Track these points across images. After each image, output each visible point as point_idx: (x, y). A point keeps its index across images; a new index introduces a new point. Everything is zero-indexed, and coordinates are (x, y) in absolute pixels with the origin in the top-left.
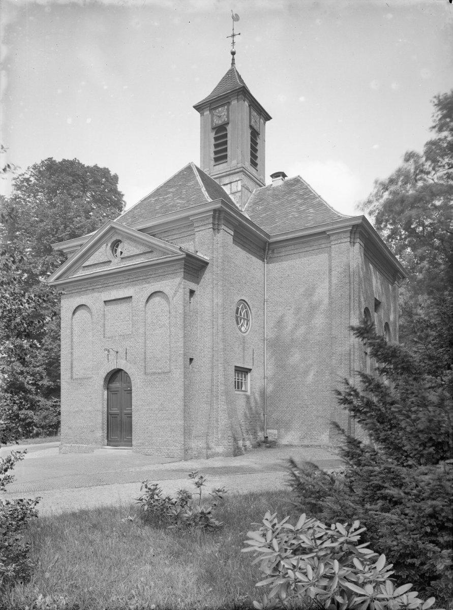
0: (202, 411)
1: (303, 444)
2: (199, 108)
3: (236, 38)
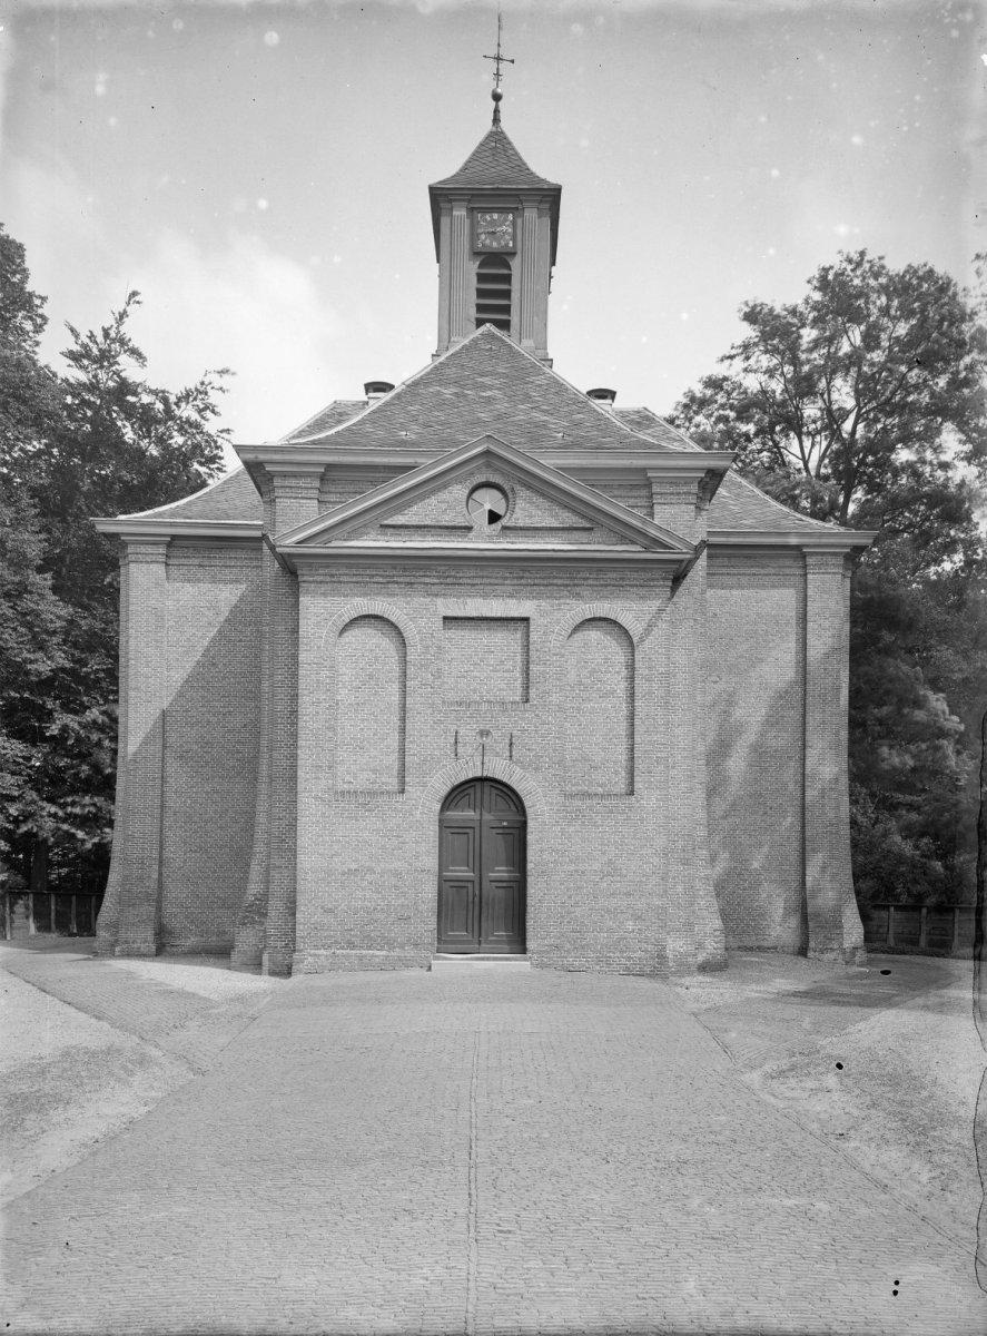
0: (674, 878)
1: (741, 944)
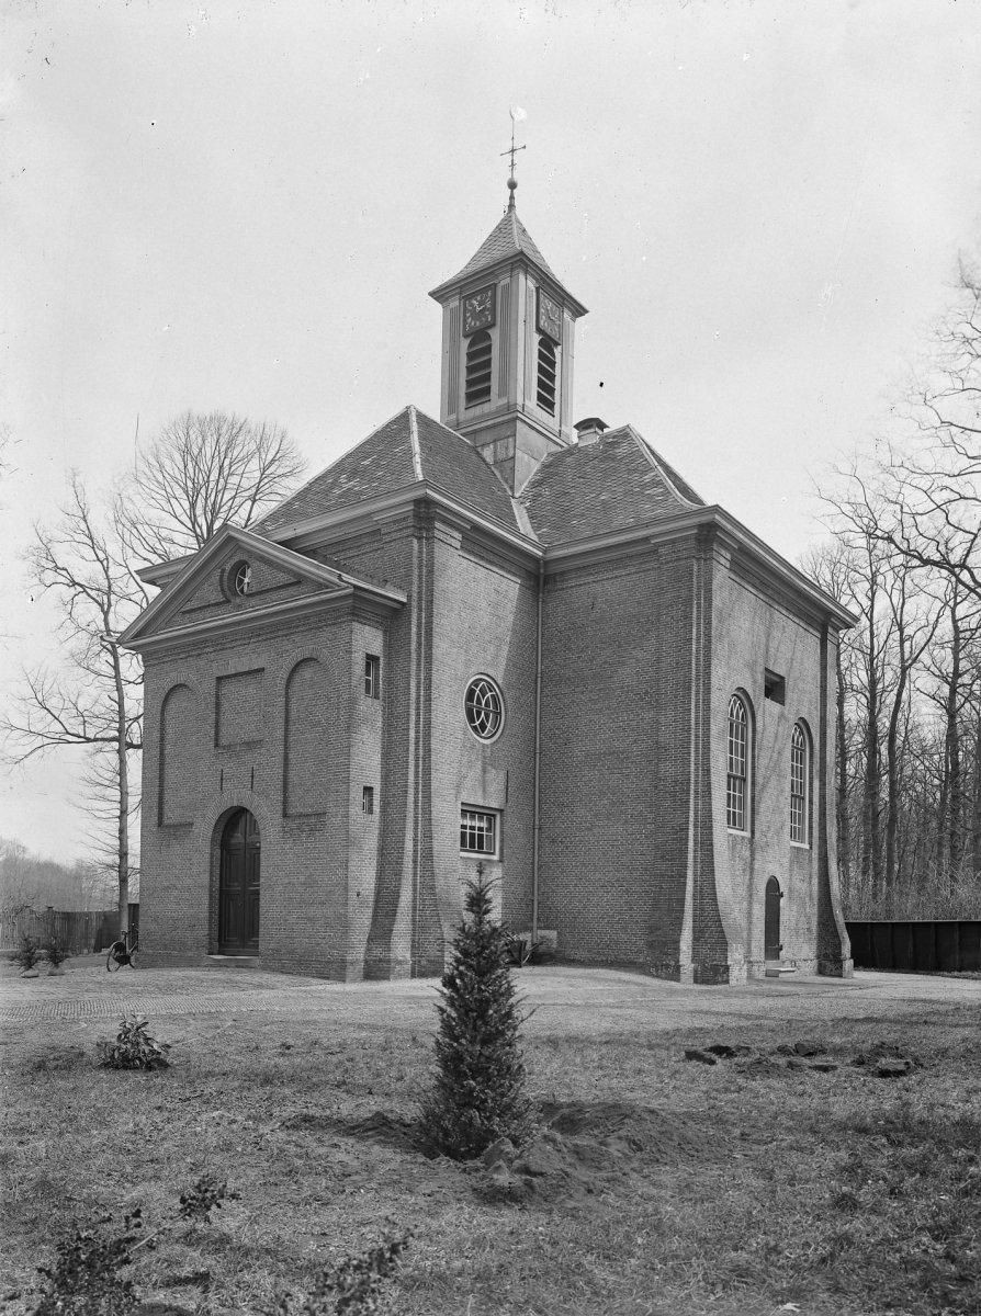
2: (440, 295)
3: (517, 154)
